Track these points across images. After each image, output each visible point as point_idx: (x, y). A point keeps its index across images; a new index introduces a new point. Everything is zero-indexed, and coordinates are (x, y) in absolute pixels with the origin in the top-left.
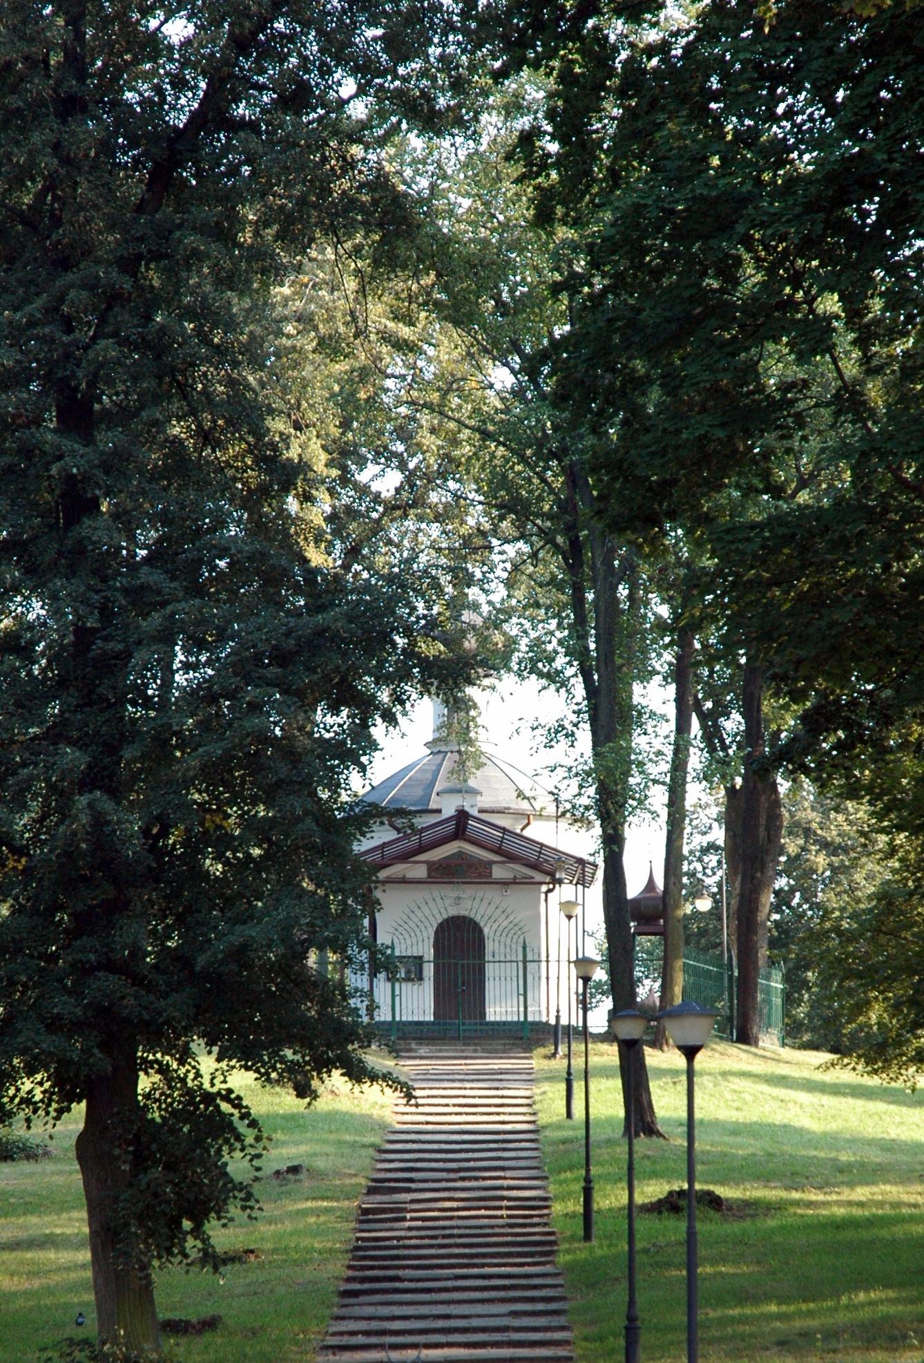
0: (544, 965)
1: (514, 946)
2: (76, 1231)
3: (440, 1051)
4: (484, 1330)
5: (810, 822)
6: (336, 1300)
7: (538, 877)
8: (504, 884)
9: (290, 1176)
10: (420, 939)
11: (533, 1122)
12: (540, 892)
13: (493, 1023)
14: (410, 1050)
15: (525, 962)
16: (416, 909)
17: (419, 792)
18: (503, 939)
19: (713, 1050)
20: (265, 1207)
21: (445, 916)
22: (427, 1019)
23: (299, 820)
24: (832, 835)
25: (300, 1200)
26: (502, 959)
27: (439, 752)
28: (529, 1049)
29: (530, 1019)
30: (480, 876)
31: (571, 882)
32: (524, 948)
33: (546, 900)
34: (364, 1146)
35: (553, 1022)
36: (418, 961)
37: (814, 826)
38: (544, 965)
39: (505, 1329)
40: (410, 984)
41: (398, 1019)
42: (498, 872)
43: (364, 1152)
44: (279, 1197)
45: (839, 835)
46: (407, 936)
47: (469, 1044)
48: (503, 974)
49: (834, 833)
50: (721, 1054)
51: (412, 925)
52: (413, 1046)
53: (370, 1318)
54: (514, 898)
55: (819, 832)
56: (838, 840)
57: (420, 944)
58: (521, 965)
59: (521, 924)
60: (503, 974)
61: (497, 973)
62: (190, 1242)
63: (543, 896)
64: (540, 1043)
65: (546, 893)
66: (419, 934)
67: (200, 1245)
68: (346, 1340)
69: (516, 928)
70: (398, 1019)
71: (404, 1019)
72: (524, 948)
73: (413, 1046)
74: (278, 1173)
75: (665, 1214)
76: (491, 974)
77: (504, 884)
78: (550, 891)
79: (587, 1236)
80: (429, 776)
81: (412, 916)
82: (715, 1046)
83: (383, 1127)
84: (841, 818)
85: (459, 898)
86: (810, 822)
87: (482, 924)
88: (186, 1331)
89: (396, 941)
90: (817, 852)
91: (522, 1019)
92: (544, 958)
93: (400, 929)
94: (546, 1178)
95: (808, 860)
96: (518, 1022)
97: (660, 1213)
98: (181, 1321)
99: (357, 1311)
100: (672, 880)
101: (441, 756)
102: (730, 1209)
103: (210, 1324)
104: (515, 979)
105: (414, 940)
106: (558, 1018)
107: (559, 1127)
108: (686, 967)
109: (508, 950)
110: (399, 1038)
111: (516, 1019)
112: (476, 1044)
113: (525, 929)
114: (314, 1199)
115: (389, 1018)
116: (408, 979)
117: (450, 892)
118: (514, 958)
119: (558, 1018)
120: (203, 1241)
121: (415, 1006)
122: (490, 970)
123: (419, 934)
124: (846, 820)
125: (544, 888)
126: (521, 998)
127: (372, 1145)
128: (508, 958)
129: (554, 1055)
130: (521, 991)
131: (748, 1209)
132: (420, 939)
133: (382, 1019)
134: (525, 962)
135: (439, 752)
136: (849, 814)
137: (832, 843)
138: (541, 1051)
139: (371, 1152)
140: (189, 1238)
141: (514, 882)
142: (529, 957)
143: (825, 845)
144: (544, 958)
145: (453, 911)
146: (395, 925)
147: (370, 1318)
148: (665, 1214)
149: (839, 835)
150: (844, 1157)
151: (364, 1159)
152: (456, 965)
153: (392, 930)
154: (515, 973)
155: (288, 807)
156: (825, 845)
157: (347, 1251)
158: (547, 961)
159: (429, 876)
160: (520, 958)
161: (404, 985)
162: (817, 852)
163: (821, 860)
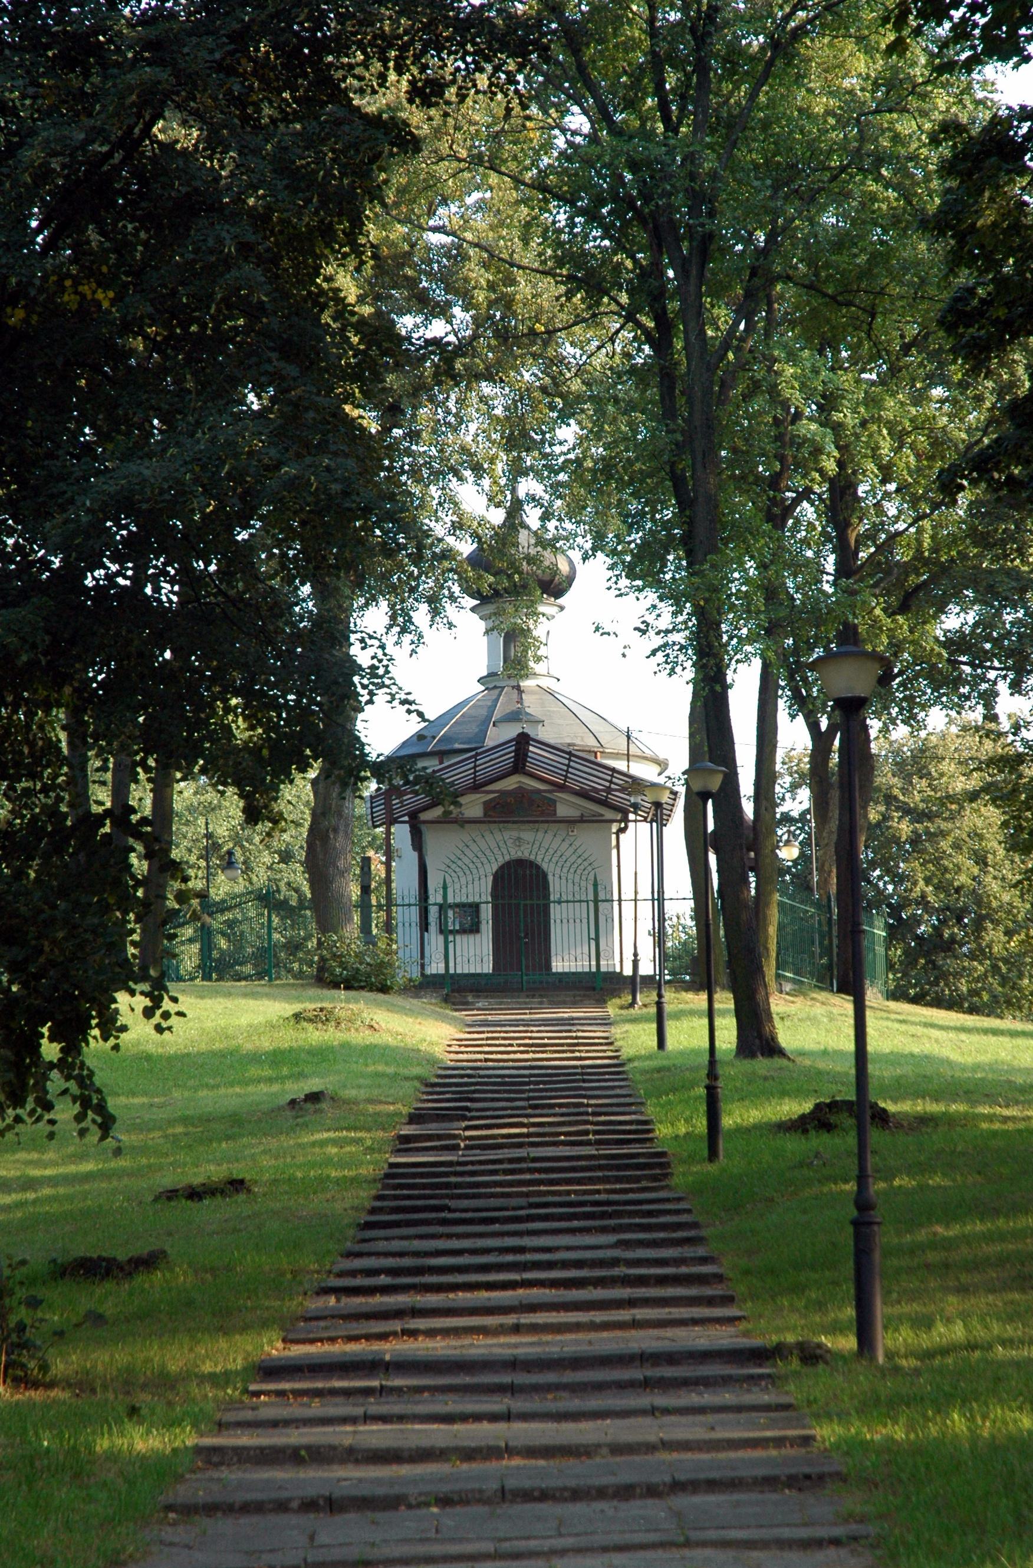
0: (616, 904)
1: (583, 884)
2: (18, 1173)
3: (501, 1003)
4: (579, 1264)
5: (891, 787)
6: (351, 1232)
7: (609, 814)
8: (570, 822)
9: (309, 1105)
10: (476, 877)
11: (617, 1057)
12: (611, 833)
13: (558, 973)
14: (467, 1003)
15: (596, 901)
16: (470, 843)
17: (473, 729)
18: (570, 876)
19: (813, 999)
20: (181, 998)
21: (507, 858)
22: (486, 971)
23: (227, 263)
24: (915, 799)
25: (318, 1131)
26: (570, 898)
27: (495, 687)
28: (601, 1002)
29: (603, 969)
30: (542, 813)
31: (645, 820)
32: (595, 885)
33: (618, 846)
34: (407, 1078)
35: (628, 971)
36: (474, 908)
37: (896, 792)
38: (616, 904)
39: (615, 1262)
40: (465, 937)
41: (452, 971)
42: (562, 811)
43: (407, 1084)
44: (292, 1129)
45: (922, 801)
46: (461, 874)
47: (533, 996)
48: (571, 916)
49: (918, 798)
50: (823, 1003)
51: (466, 860)
52: (470, 999)
53: (401, 1254)
54: (585, 838)
55: (901, 798)
56: (922, 806)
57: (476, 883)
58: (591, 904)
59: (592, 859)
60: (571, 916)
61: (564, 915)
62: (56, 1081)
63: (614, 836)
64: (615, 993)
65: (617, 834)
66: (475, 871)
67: (73, 1086)
68: (359, 1281)
69: (586, 864)
70: (452, 971)
71: (459, 971)
72: (595, 885)
73: (470, 999)
74: (293, 1102)
75: (812, 1133)
76: (558, 916)
77: (570, 822)
78: (622, 830)
79: (713, 1153)
80: (484, 712)
81: (467, 851)
82: (814, 995)
83: (431, 1061)
84: (924, 782)
85: (519, 839)
86: (891, 787)
87: (545, 866)
88: (107, 1274)
89: (448, 880)
90: (900, 818)
91: (594, 969)
92: (616, 897)
93: (453, 866)
94: (642, 1104)
95: (890, 827)
96: (590, 973)
97: (805, 1131)
98: (101, 1259)
99: (382, 1246)
100: (764, 803)
101: (497, 691)
102: (899, 1126)
103: (147, 1262)
104: (585, 921)
105: (470, 878)
106: (635, 963)
107: (650, 1057)
108: (781, 904)
109: (577, 888)
110: (453, 991)
111: (587, 970)
112: (541, 996)
113: (595, 865)
114: (336, 1130)
115: (442, 971)
116: (463, 931)
117: (510, 834)
118: (583, 898)
119: (635, 963)
120: (81, 1081)
121: (472, 953)
122: (555, 911)
123: (475, 871)
124: (930, 785)
125: (615, 828)
126: (593, 943)
127: (419, 1078)
128: (577, 898)
129: (632, 1005)
130: (593, 935)
131: (924, 1120)
132: (476, 877)
133: (434, 972)
134: (596, 901)
135: (495, 687)
136: (933, 779)
137: (916, 808)
138: (617, 1001)
139: (417, 1084)
140: (55, 1074)
141: (582, 820)
142: (601, 896)
143: (907, 811)
144: (616, 897)
145: (516, 854)
146: (447, 861)
147: (401, 1254)
148: (812, 1133)
149: (922, 801)
150: (1020, 1080)
151: (409, 1088)
152: (517, 906)
153: (443, 867)
154: (585, 915)
155: (211, 242)
156: (907, 811)
157: (375, 1181)
158: (620, 900)
159: (485, 815)
160: (591, 897)
161: (458, 938)
162: (900, 818)
163: (904, 828)
